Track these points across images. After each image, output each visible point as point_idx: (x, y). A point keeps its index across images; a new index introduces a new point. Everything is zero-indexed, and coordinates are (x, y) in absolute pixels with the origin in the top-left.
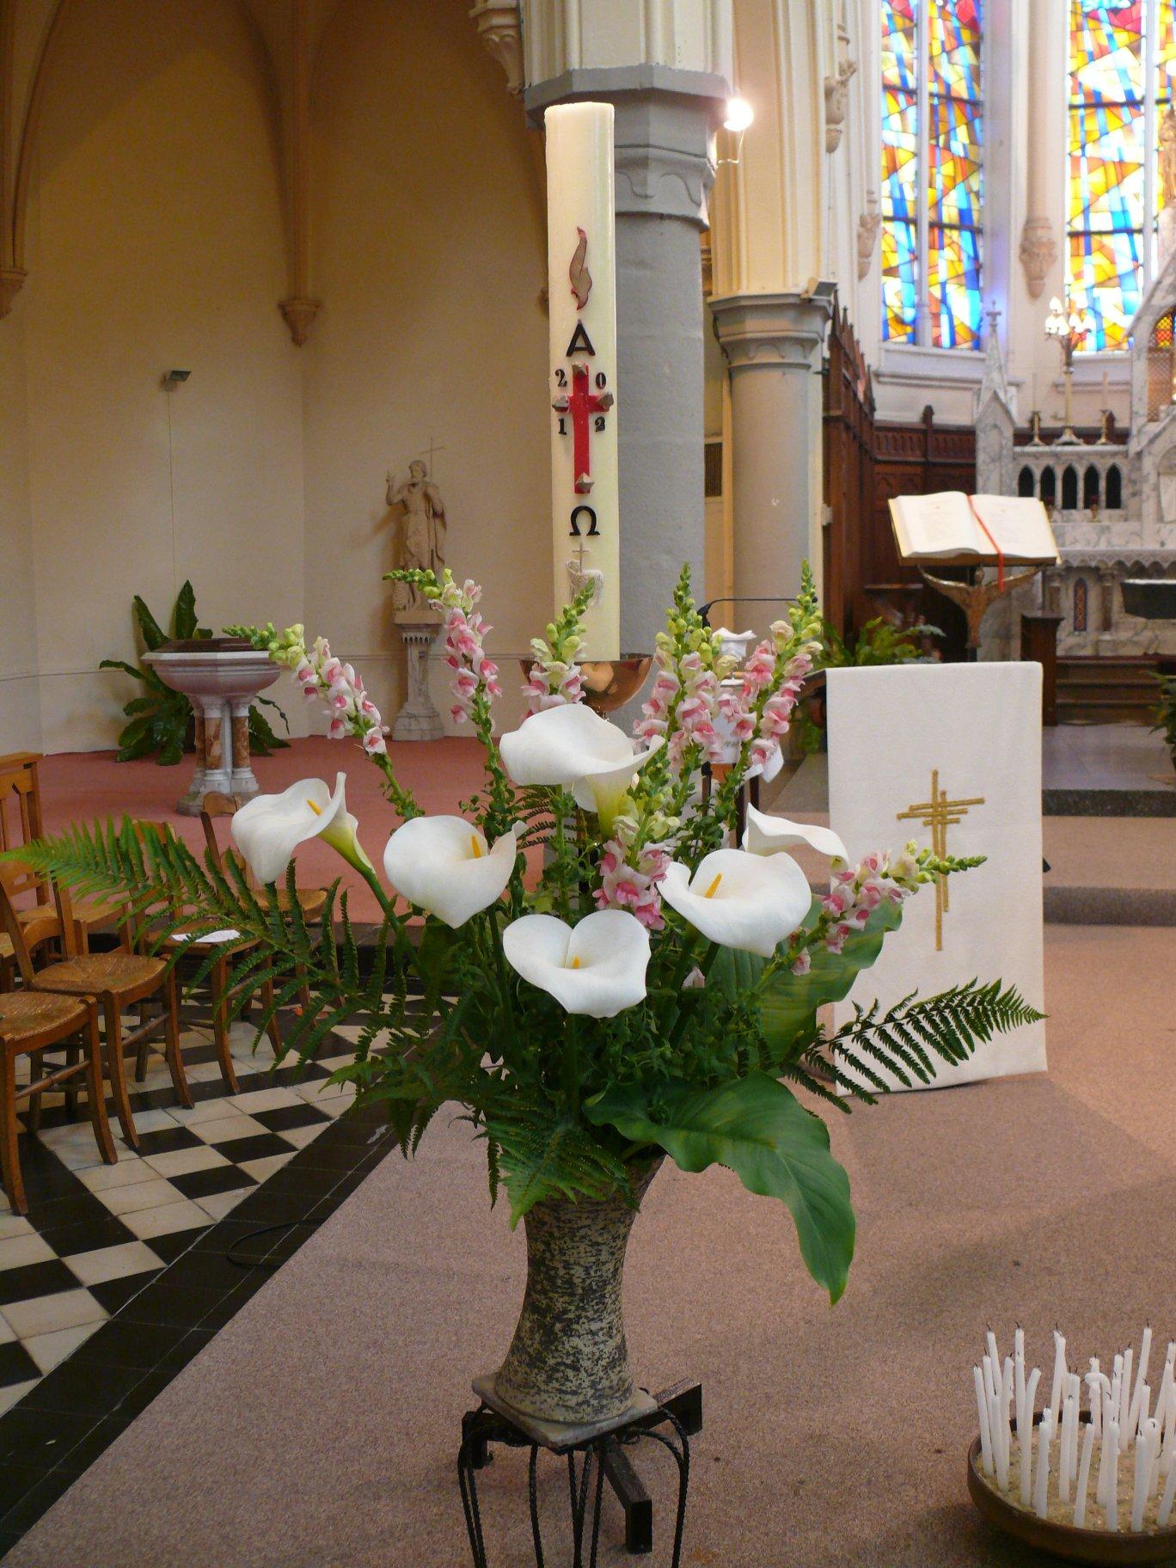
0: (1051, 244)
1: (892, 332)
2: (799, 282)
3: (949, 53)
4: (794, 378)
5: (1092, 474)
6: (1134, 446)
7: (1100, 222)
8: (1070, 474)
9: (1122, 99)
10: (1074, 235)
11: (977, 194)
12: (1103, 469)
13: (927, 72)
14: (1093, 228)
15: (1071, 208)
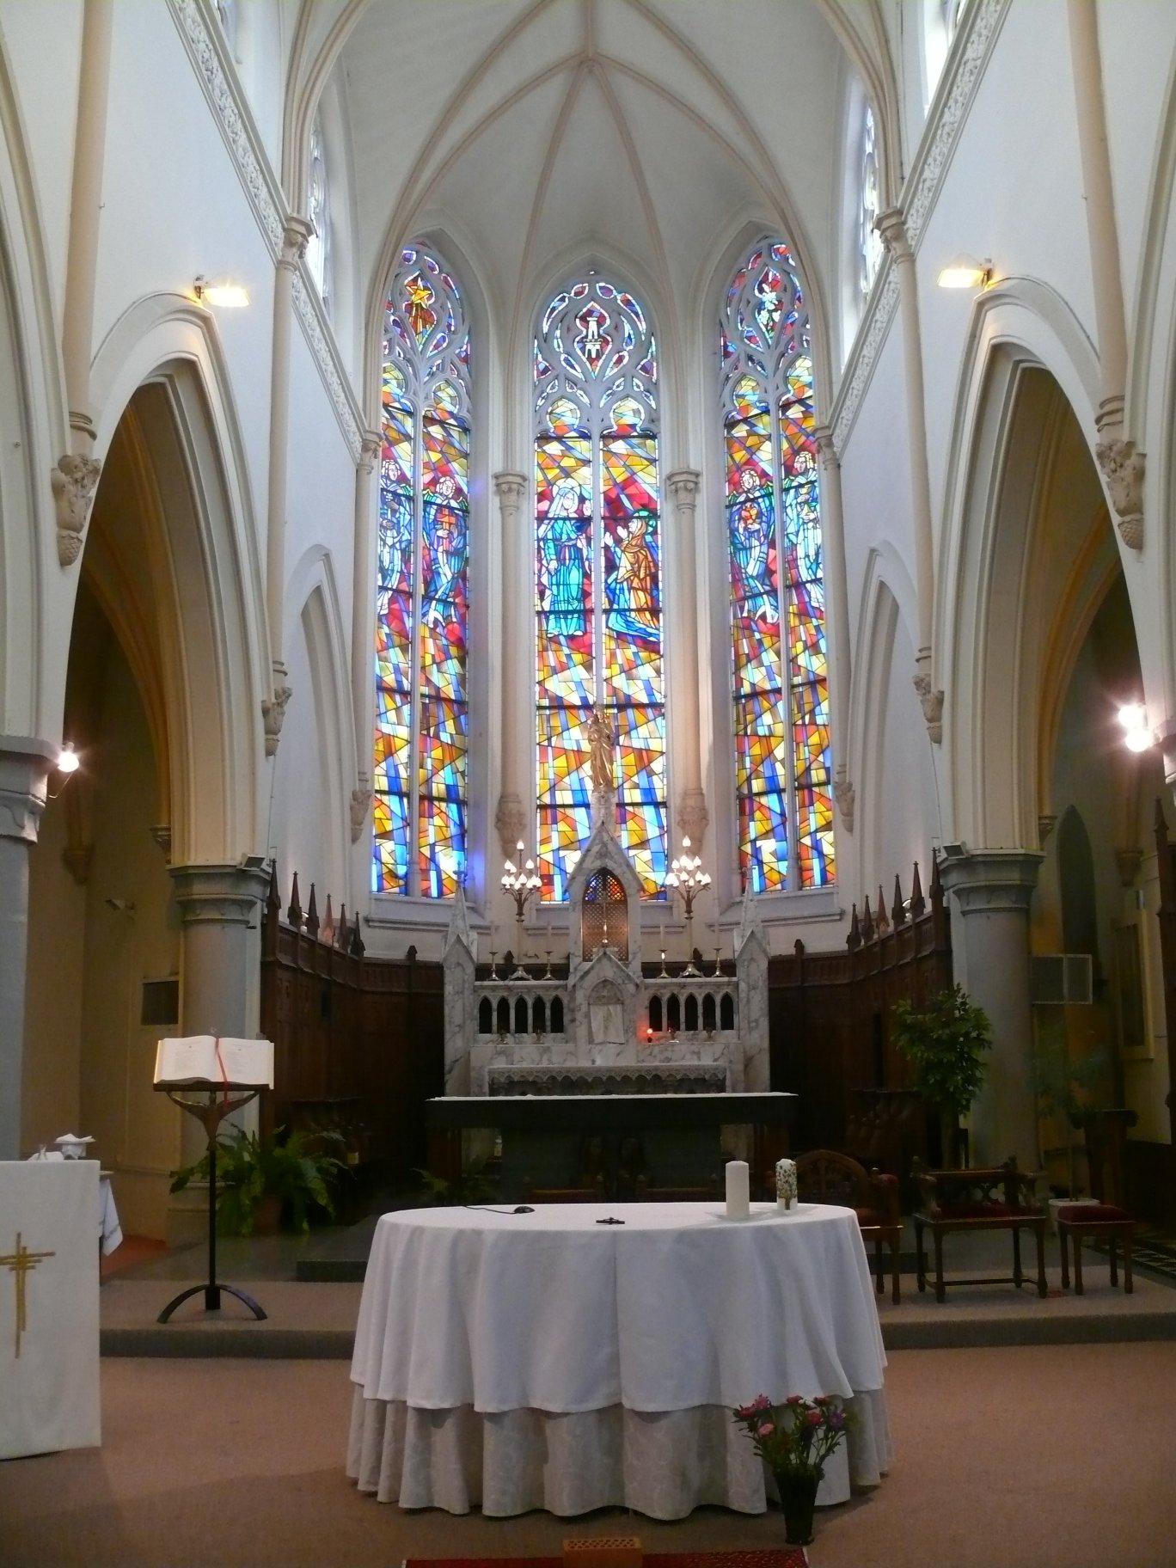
0: (521, 815)
1: (386, 884)
2: (234, 856)
3: (438, 664)
4: (233, 932)
5: (539, 1002)
6: (571, 981)
7: (564, 797)
8: (521, 1004)
9: (578, 703)
10: (543, 807)
11: (463, 773)
12: (548, 998)
13: (420, 678)
14: (559, 801)
15: (541, 785)
